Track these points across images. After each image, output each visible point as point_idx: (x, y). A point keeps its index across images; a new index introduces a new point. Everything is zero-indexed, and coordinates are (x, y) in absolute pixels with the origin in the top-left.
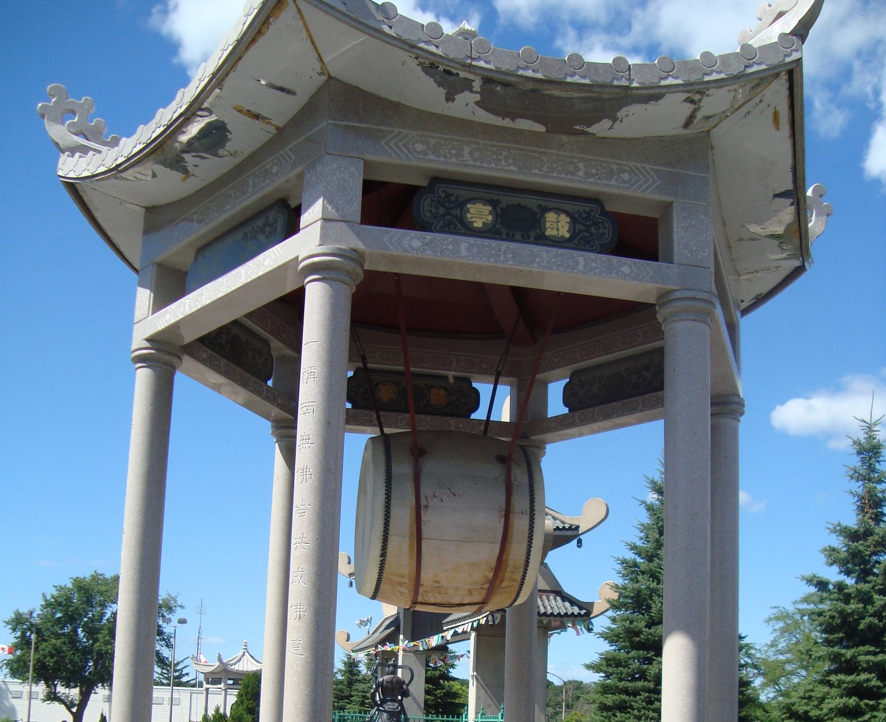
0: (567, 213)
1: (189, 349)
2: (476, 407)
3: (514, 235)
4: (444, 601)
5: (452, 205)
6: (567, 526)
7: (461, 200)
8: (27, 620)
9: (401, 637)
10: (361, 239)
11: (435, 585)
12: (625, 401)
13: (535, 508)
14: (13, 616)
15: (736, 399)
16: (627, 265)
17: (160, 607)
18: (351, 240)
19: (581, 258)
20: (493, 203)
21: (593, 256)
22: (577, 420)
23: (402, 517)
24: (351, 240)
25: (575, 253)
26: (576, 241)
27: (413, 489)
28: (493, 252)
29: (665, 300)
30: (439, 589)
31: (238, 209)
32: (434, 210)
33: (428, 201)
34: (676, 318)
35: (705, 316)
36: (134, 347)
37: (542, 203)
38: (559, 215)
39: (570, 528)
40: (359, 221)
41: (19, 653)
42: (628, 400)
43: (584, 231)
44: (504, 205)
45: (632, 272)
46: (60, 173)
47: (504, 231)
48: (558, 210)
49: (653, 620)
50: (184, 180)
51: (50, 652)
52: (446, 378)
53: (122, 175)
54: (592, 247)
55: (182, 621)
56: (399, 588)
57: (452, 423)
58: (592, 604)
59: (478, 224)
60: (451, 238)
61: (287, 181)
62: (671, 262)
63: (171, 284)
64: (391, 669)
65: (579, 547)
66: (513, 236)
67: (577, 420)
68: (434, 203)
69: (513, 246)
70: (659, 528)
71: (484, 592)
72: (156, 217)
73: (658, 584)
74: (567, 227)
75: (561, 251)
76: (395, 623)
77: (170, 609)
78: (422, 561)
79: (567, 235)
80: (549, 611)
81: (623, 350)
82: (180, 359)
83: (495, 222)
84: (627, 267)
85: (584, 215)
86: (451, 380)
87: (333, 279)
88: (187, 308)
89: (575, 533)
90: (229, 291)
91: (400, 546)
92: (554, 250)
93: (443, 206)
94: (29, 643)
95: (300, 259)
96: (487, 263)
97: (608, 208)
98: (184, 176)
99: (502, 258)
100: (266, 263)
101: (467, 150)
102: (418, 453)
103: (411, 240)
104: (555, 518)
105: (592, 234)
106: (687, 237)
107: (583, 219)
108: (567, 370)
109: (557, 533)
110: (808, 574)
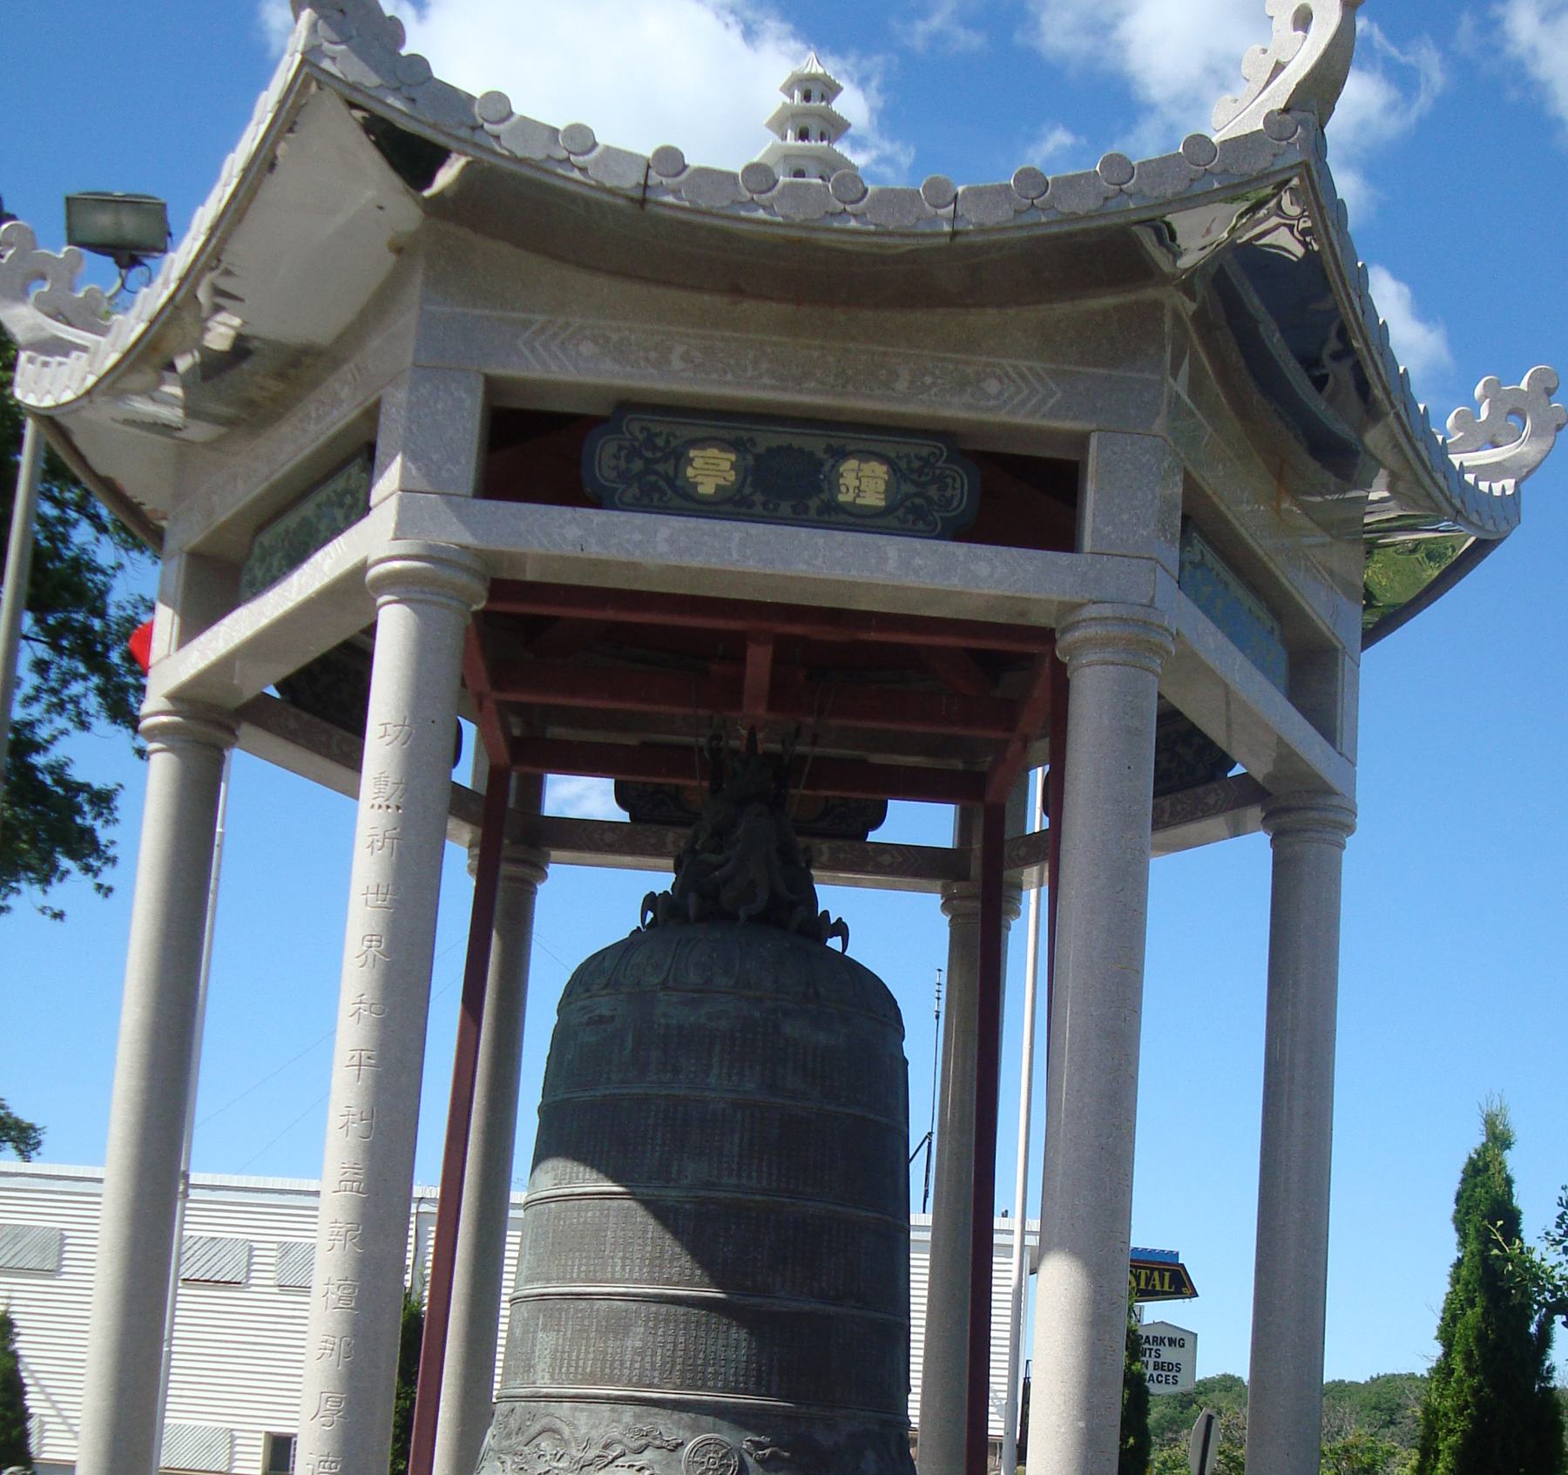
1: (257, 712)
5: (659, 454)
18: (454, 532)
21: (917, 543)
29: (1071, 619)
32: (623, 464)
33: (611, 448)
40: (470, 491)
44: (761, 449)
47: (758, 498)
48: (866, 455)
59: (707, 488)
60: (639, 518)
66: (776, 509)
68: (624, 453)
85: (916, 464)
87: (420, 601)
93: (641, 457)
101: (679, 349)
105: (929, 500)
110: (1518, 1125)
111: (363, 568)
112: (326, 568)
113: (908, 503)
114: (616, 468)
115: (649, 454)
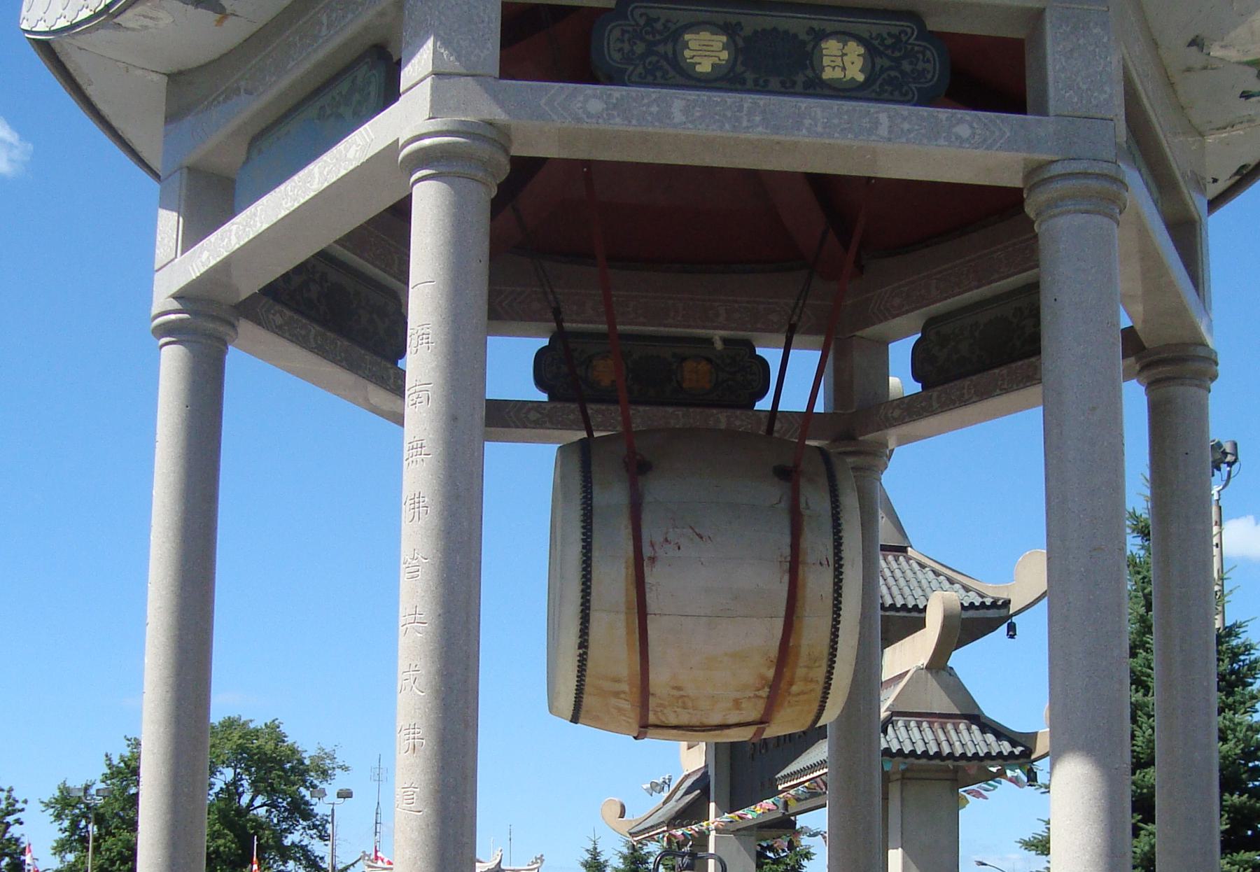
0: (860, 40)
1: (250, 309)
2: (762, 394)
3: (766, 82)
4: (694, 721)
5: (658, 37)
6: (988, 601)
7: (673, 27)
8: (80, 800)
9: (712, 806)
10: (502, 105)
11: (676, 693)
12: (1013, 365)
13: (843, 554)
14: (57, 794)
15: (1201, 352)
16: (966, 122)
17: (307, 771)
18: (483, 107)
19: (883, 115)
20: (728, 29)
21: (905, 110)
22: (935, 405)
23: (612, 579)
24: (483, 107)
25: (873, 107)
26: (876, 87)
27: (630, 530)
28: (729, 114)
29: (1036, 179)
30: (682, 700)
31: (307, 65)
32: (626, 47)
33: (617, 33)
34: (1056, 211)
35: (1109, 201)
36: (155, 311)
37: (815, 24)
38: (845, 44)
39: (994, 605)
40: (496, 72)
41: (71, 857)
42: (1020, 363)
43: (890, 68)
44: (747, 31)
45: (974, 134)
46: (25, 26)
47: (749, 76)
48: (844, 36)
49: (1139, 759)
50: (220, 22)
51: (120, 853)
52: (709, 341)
53: (116, 20)
54: (905, 95)
55: (345, 795)
56: (613, 701)
57: (722, 419)
58: (1034, 736)
59: (705, 67)
60: (654, 93)
61: (382, 14)
62: (1042, 111)
63: (210, 199)
64: (686, 860)
65: (1012, 637)
67: (935, 405)
68: (626, 36)
69: (762, 100)
70: (1145, 596)
71: (761, 705)
72: (186, 89)
73: (1145, 695)
74: (859, 63)
75: (848, 105)
76: (702, 783)
77: (325, 774)
78: (650, 648)
79: (861, 78)
80: (959, 751)
81: (1008, 277)
82: (233, 326)
83: (733, 62)
84: (966, 126)
85: (889, 41)
86: (719, 345)
88: (234, 240)
89: (1003, 612)
90: (296, 205)
91: (611, 628)
92: (836, 104)
94: (84, 840)
95: (401, 143)
96: (719, 133)
97: (933, 25)
98: (218, 16)
99: (745, 124)
100: (351, 155)
102: (638, 468)
103: (586, 101)
104: (967, 589)
105: (903, 73)
106: (1079, 72)
107: (887, 47)
108: (916, 318)
109: (971, 614)
111: (394, 147)
112: (206, 254)
113: (885, 76)
114: (620, 50)
115: (650, 37)
